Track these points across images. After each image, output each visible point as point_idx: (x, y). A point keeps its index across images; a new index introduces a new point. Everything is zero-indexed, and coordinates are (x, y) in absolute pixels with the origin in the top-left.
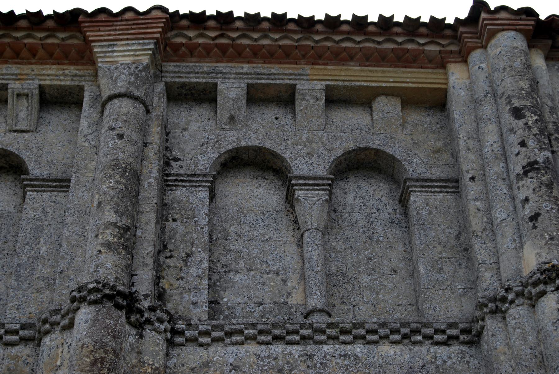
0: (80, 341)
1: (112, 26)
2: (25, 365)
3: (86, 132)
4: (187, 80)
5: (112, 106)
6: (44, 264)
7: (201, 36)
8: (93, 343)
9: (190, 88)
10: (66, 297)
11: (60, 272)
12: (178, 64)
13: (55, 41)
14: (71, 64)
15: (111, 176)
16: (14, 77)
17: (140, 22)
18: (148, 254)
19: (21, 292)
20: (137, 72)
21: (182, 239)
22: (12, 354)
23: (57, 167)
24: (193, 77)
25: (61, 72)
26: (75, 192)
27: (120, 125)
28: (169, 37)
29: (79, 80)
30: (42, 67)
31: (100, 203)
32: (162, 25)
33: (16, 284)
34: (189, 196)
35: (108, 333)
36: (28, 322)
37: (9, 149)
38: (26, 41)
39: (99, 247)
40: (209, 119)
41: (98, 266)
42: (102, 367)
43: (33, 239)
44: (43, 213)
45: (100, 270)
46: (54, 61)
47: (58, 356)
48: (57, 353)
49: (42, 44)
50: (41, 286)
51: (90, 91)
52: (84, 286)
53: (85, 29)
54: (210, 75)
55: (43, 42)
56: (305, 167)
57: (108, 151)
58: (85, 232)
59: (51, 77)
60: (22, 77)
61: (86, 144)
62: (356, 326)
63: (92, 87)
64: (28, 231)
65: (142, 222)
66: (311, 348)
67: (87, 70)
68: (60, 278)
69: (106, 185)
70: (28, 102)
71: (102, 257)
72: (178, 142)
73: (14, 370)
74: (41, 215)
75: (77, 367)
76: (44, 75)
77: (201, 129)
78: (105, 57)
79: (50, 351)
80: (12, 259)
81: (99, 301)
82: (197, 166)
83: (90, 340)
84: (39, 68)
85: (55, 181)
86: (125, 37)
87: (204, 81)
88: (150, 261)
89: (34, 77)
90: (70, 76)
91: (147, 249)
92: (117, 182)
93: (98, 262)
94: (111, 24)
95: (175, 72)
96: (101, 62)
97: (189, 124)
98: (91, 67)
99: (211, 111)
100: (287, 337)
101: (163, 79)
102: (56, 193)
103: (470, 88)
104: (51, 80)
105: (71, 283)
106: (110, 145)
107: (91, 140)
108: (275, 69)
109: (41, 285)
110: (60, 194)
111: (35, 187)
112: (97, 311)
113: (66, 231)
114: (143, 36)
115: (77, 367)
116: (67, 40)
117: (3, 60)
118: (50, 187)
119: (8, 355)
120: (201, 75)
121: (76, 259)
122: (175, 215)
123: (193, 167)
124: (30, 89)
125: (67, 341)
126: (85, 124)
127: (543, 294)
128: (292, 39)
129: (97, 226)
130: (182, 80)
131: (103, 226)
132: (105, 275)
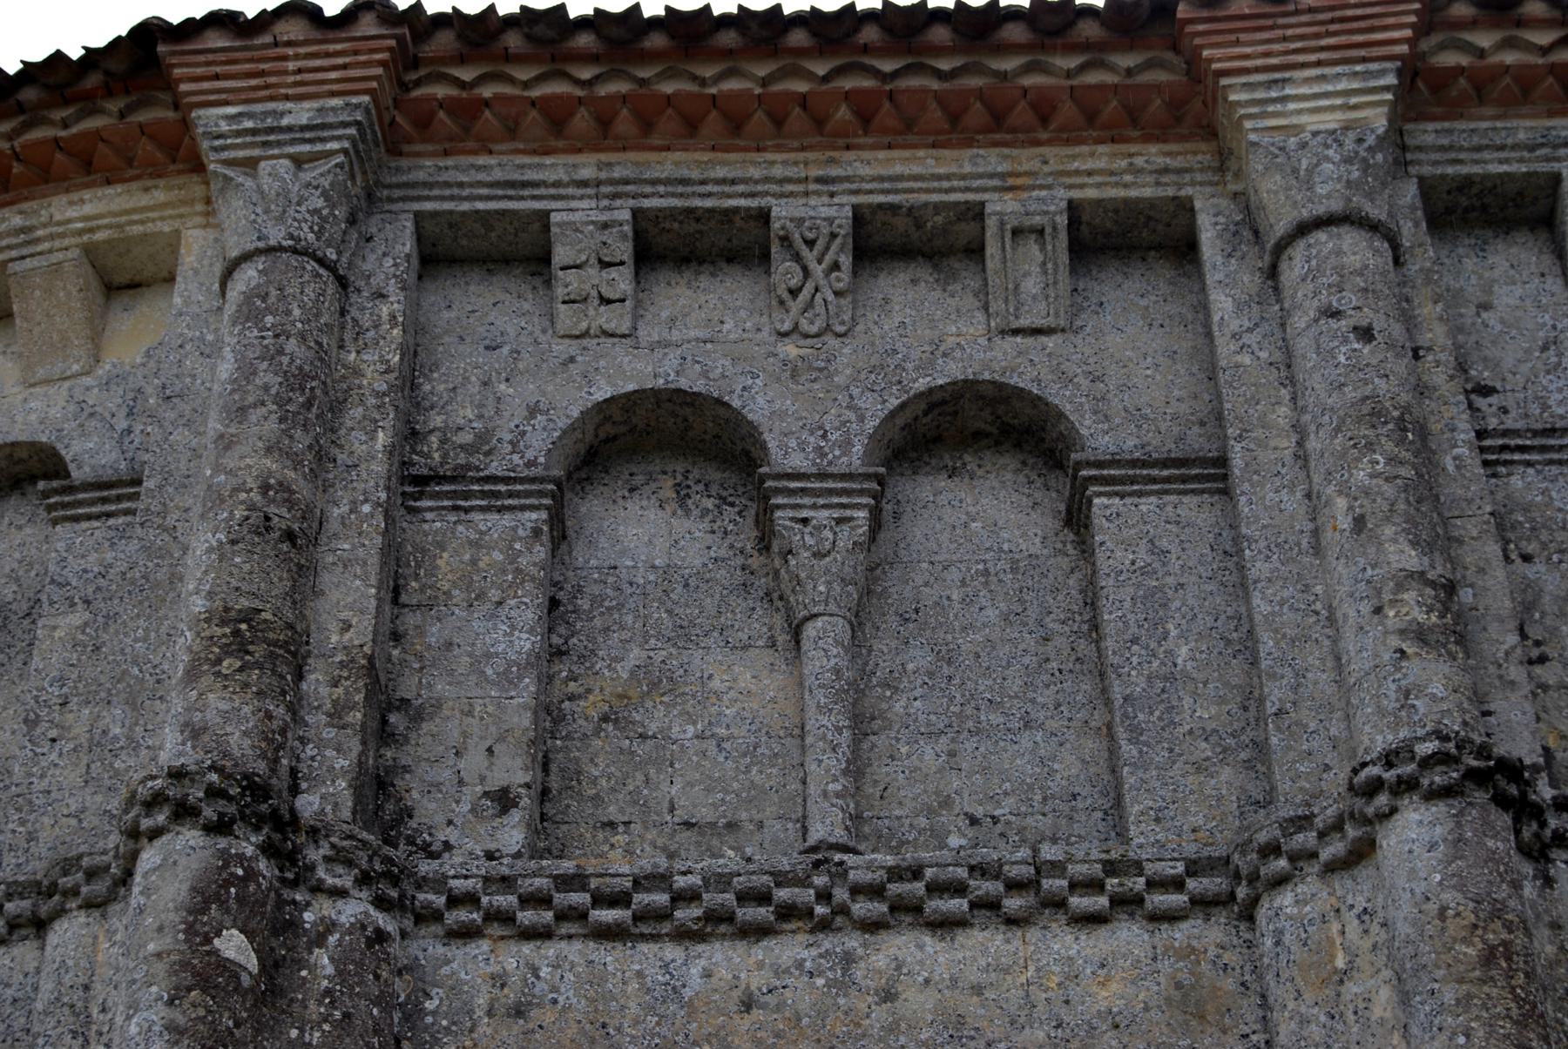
0: (1428, 899)
1: (1272, 28)
2: (1221, 972)
3: (1234, 325)
4: (1477, 169)
5: (1314, 252)
6: (1195, 695)
7: (1508, 44)
8: (1471, 905)
9: (1482, 191)
10: (1310, 782)
11: (1276, 714)
12: (1446, 125)
13: (1109, 78)
14: (1148, 139)
15: (1371, 444)
16: (996, 182)
17: (1350, 13)
18: (1507, 653)
19: (1154, 773)
20: (1363, 154)
21: (1560, 609)
22: (1177, 944)
23: (1156, 426)
24: (1491, 161)
25: (1124, 163)
26: (1255, 493)
27: (1354, 303)
28: (1424, 53)
29: (1176, 184)
30: (1069, 151)
31: (1359, 522)
32: (1413, 19)
33: (1135, 753)
34: (1547, 489)
35: (1500, 875)
36: (1205, 853)
37: (1012, 382)
38: (1028, 81)
39: (1394, 642)
40: (1543, 275)
41: (1407, 695)
42: (1510, 968)
43: (1146, 626)
44: (1153, 554)
45: (1415, 702)
46: (1101, 133)
47: (1334, 943)
48: (1328, 937)
49: (1072, 88)
50: (1203, 756)
51: (1211, 212)
52: (1402, 748)
53: (1197, 41)
54: (1538, 153)
55: (1075, 82)
57: (1340, 375)
58: (1314, 602)
59: (1099, 179)
60: (1019, 181)
61: (1246, 359)
63: (1215, 200)
64: (1127, 604)
65: (1466, 568)
67: (1195, 153)
68: (1279, 729)
69: (1363, 470)
70: (1043, 249)
71: (1414, 670)
72: (1477, 343)
73: (1193, 987)
74: (1149, 561)
75: (1442, 972)
76: (1077, 172)
77: (1528, 302)
78: (1264, 115)
79: (1306, 931)
80: (1078, 684)
81: (1456, 788)
82: (1545, 407)
83: (1459, 896)
84: (1063, 154)
85: (1165, 463)
86: (1313, 58)
87: (1524, 170)
89: (1050, 180)
90: (1151, 172)
91: (1501, 640)
92: (1390, 460)
93: (1403, 682)
94: (1269, 22)
95: (1442, 149)
96: (1255, 130)
97: (1491, 293)
98: (1203, 146)
99: (1541, 252)
100: (592, 912)
101: (1413, 170)
102: (1173, 498)
104: (1098, 185)
105: (1315, 743)
106: (1342, 359)
107: (1255, 346)
109: (1203, 751)
110: (1186, 499)
111: (1114, 485)
112: (1454, 815)
113: (1259, 601)
114: (1363, 53)
115: (1442, 972)
116: (1139, 72)
117: (962, 136)
118: (1154, 480)
119: (1164, 946)
120: (1513, 155)
121: (1309, 675)
122: (1524, 543)
123: (1535, 409)
124: (1046, 213)
125: (1350, 902)
126: (1225, 305)
128: (810, 76)
129: (1369, 582)
130: (1465, 170)
131: (1391, 584)
132: (1434, 717)
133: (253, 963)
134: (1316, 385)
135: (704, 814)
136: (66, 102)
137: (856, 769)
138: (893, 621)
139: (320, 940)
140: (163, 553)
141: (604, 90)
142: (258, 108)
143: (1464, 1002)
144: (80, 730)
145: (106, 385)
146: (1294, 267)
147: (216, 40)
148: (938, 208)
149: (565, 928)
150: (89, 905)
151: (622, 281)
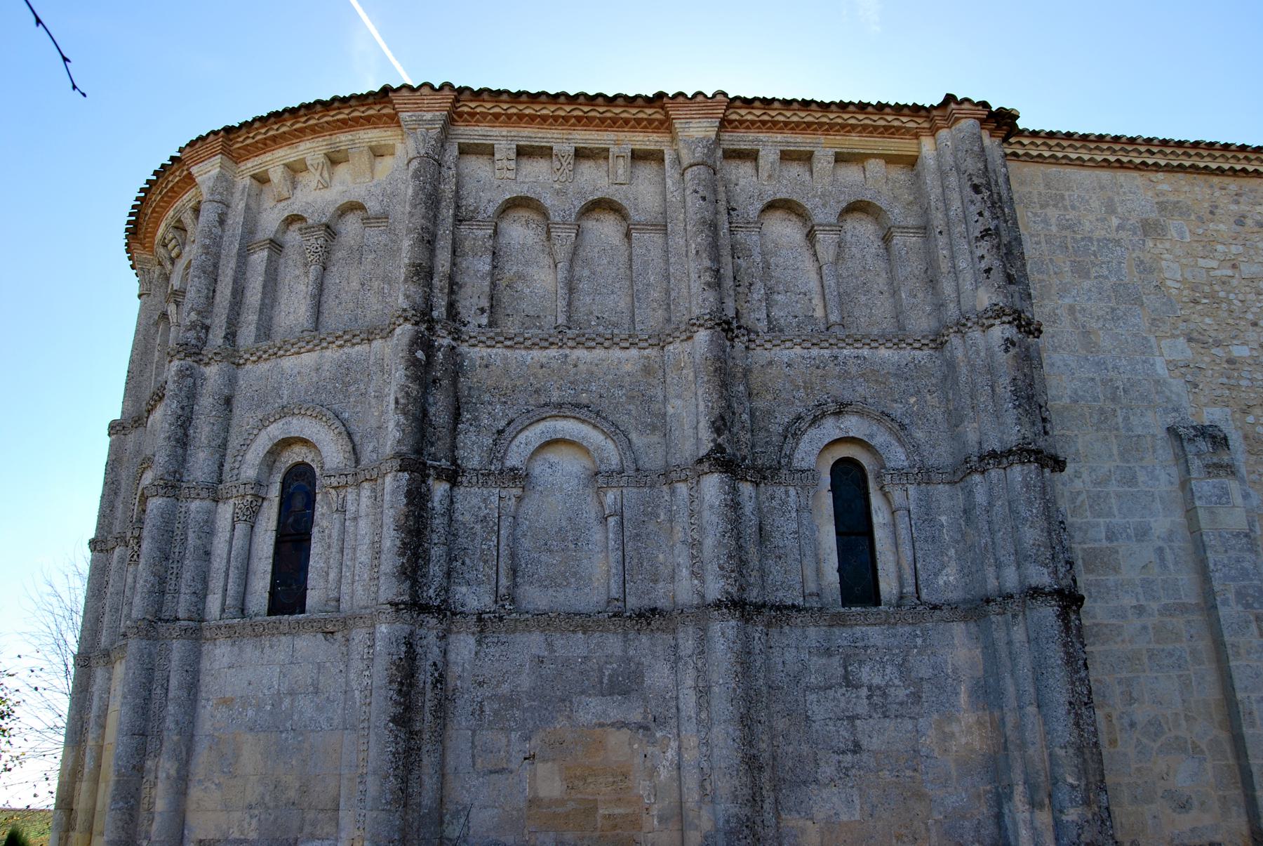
13: (645, 116)
31: (697, 252)
56: (821, 216)
62: (863, 337)
66: (835, 351)
88: (732, 292)
103: (939, 155)
108: (800, 138)
127: (992, 325)
130: (735, 147)
133: (424, 358)
134: (691, 211)
135: (532, 313)
136: (363, 105)
137: (569, 304)
138: (580, 262)
139: (439, 350)
140: (395, 242)
141: (510, 111)
142: (417, 113)
143: (709, 381)
144: (375, 287)
145: (376, 186)
146: (688, 175)
147: (405, 93)
148: (597, 148)
149: (499, 345)
150: (382, 338)
151: (513, 165)
